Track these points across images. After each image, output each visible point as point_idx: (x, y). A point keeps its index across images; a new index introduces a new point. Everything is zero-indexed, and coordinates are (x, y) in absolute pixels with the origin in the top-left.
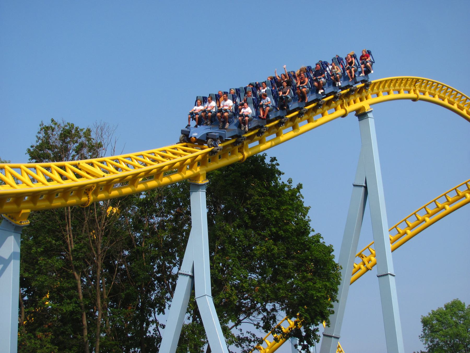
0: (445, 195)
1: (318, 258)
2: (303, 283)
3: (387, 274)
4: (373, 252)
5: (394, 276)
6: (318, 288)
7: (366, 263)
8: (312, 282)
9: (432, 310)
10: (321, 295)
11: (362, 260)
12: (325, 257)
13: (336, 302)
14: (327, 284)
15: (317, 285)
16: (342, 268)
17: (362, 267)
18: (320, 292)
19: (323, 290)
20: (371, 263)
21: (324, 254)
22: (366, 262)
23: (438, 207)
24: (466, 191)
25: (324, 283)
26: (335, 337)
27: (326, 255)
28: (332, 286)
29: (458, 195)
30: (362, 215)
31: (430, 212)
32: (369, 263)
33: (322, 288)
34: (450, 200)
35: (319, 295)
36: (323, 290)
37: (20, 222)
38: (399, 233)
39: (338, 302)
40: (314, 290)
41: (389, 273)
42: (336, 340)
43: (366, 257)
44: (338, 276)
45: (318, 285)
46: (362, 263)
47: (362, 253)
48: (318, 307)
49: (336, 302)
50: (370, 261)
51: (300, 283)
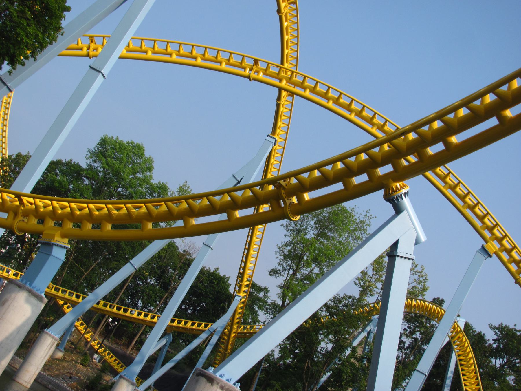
0: (206, 48)
1: (50, 5)
2: (18, 16)
3: (99, 72)
4: (105, 43)
5: (104, 77)
6: (29, 32)
7: (91, 49)
8: (27, 22)
9: (117, 137)
10: (26, 41)
11: (90, 44)
12: (57, 10)
13: (33, 59)
14: (40, 35)
15: (30, 29)
16: (62, 35)
17: (85, 49)
18: (27, 36)
19: (32, 37)
20: (95, 53)
21: (59, 7)
22: (92, 48)
23: (191, 53)
24: (213, 57)
25: (38, 32)
26: (8, 87)
27: (59, 9)
28: (43, 41)
29: (216, 57)
30: (119, 4)
31: (182, 52)
32: (93, 51)
33: (32, 35)
34: (207, 56)
35: (25, 39)
36: (32, 37)
37: (475, 380)
38: (141, 47)
39: (35, 60)
40: (24, 31)
41: (102, 71)
42: (7, 90)
43: (95, 44)
44: (53, 40)
45: (30, 30)
46: (87, 46)
47: (95, 38)
48: (14, 49)
49: (33, 59)
50: (96, 49)
51: (15, 14)
